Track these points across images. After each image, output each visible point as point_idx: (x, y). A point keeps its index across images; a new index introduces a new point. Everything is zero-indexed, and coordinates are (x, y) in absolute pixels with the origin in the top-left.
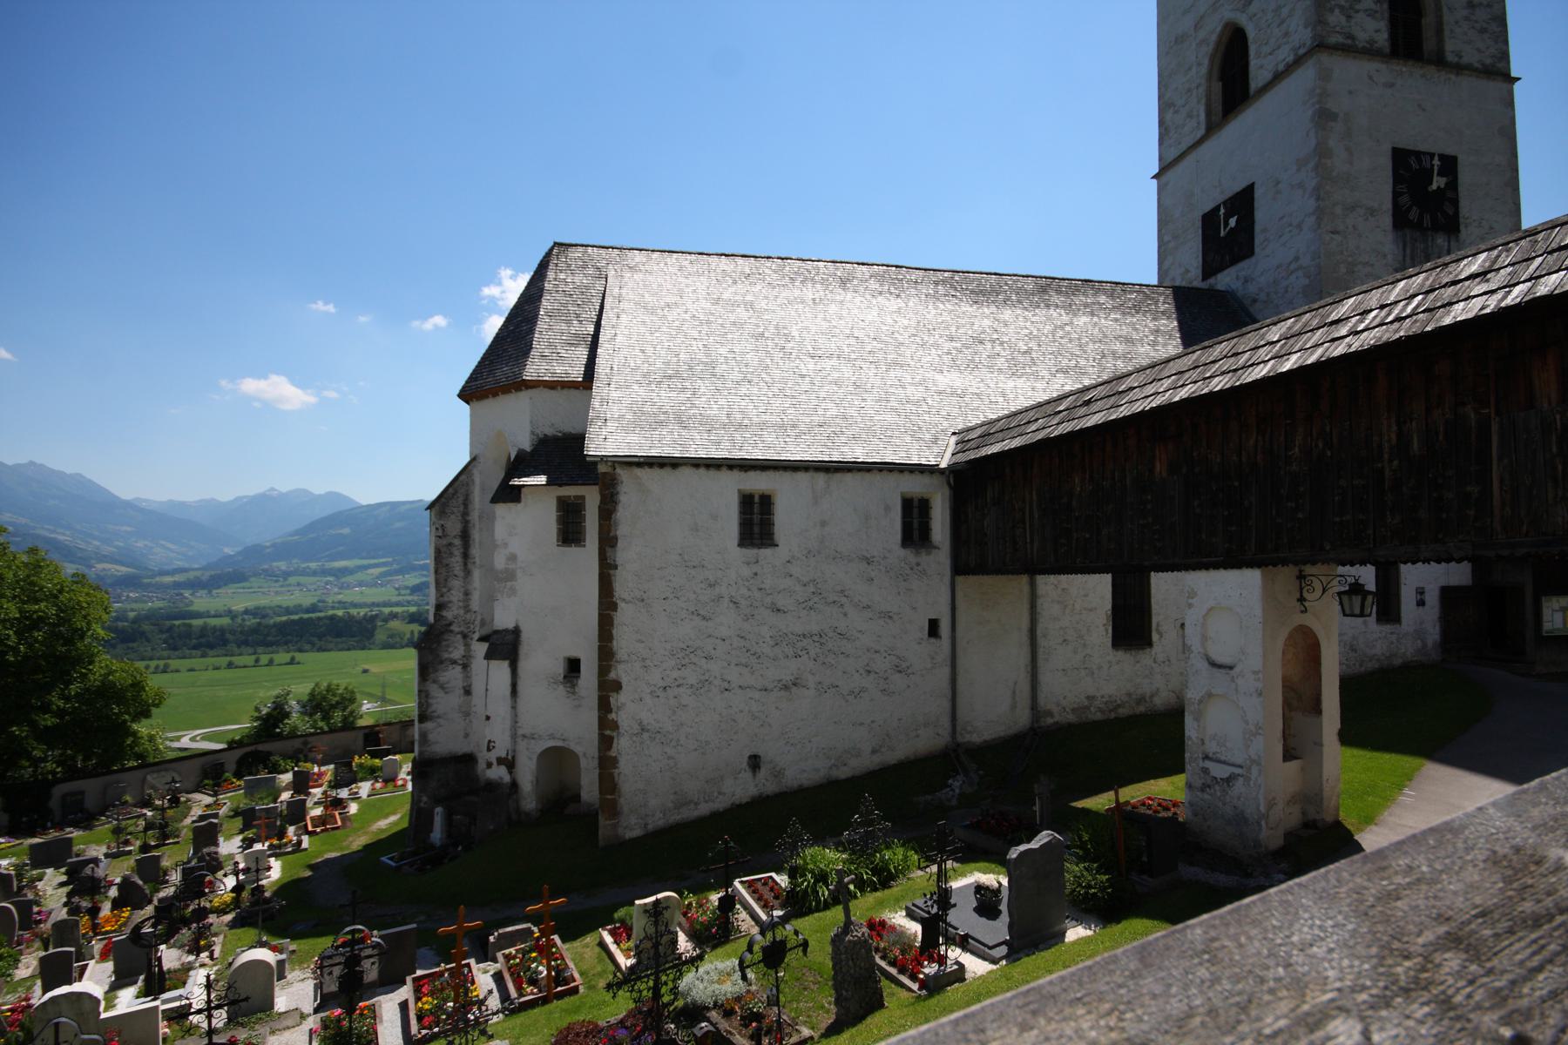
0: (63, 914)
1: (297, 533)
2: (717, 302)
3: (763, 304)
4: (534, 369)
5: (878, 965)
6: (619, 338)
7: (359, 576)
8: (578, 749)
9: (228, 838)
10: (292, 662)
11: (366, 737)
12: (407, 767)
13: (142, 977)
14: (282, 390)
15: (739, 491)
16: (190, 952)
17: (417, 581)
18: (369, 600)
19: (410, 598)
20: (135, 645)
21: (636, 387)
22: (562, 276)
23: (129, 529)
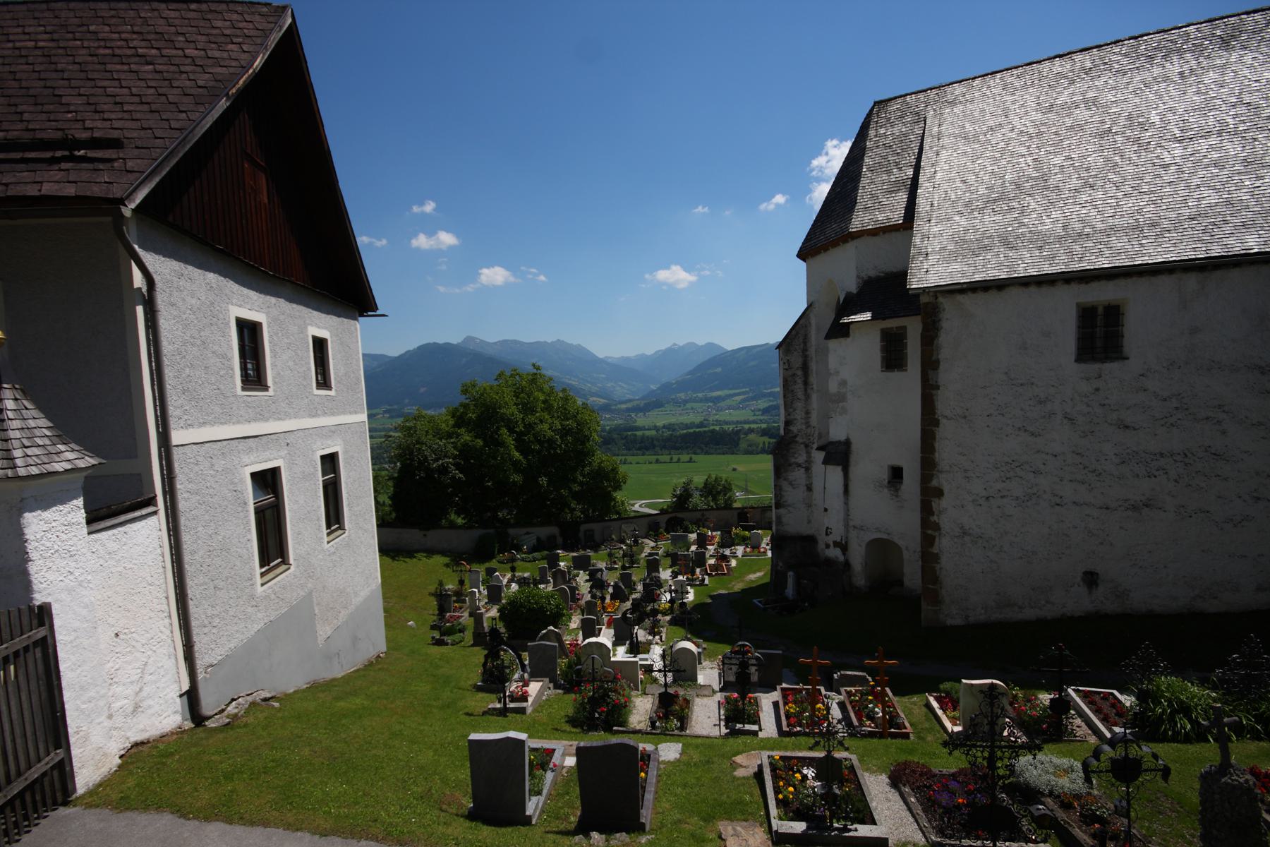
0: (588, 597)
1: (690, 373)
2: (1050, 109)
3: (1110, 97)
4: (860, 220)
5: (1264, 818)
6: (939, 175)
7: (728, 402)
8: (901, 543)
9: (664, 569)
10: (690, 461)
11: (739, 514)
12: (766, 540)
13: (628, 642)
14: (677, 275)
15: (1078, 305)
16: (650, 634)
17: (766, 405)
18: (734, 419)
19: (762, 418)
20: (610, 446)
21: (957, 218)
22: (882, 131)
23: (603, 376)
